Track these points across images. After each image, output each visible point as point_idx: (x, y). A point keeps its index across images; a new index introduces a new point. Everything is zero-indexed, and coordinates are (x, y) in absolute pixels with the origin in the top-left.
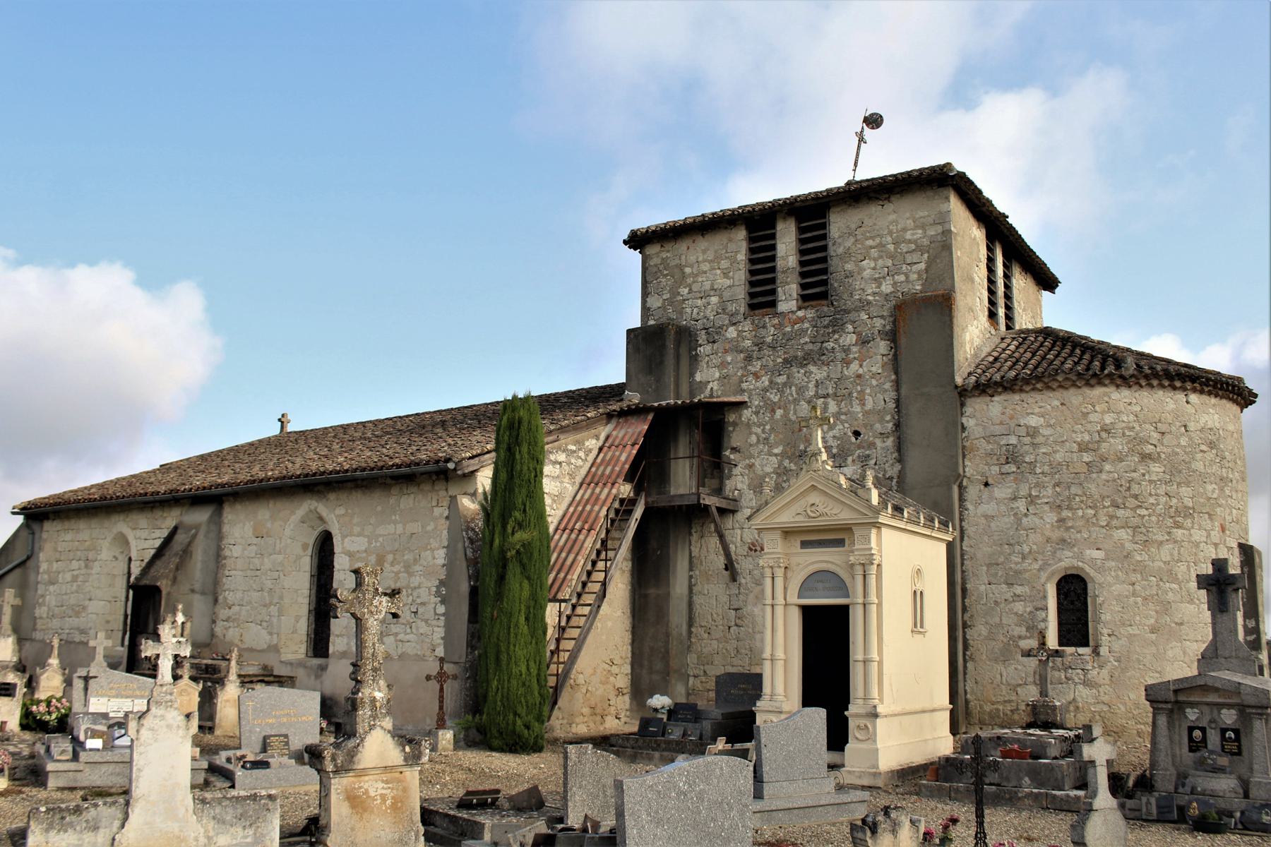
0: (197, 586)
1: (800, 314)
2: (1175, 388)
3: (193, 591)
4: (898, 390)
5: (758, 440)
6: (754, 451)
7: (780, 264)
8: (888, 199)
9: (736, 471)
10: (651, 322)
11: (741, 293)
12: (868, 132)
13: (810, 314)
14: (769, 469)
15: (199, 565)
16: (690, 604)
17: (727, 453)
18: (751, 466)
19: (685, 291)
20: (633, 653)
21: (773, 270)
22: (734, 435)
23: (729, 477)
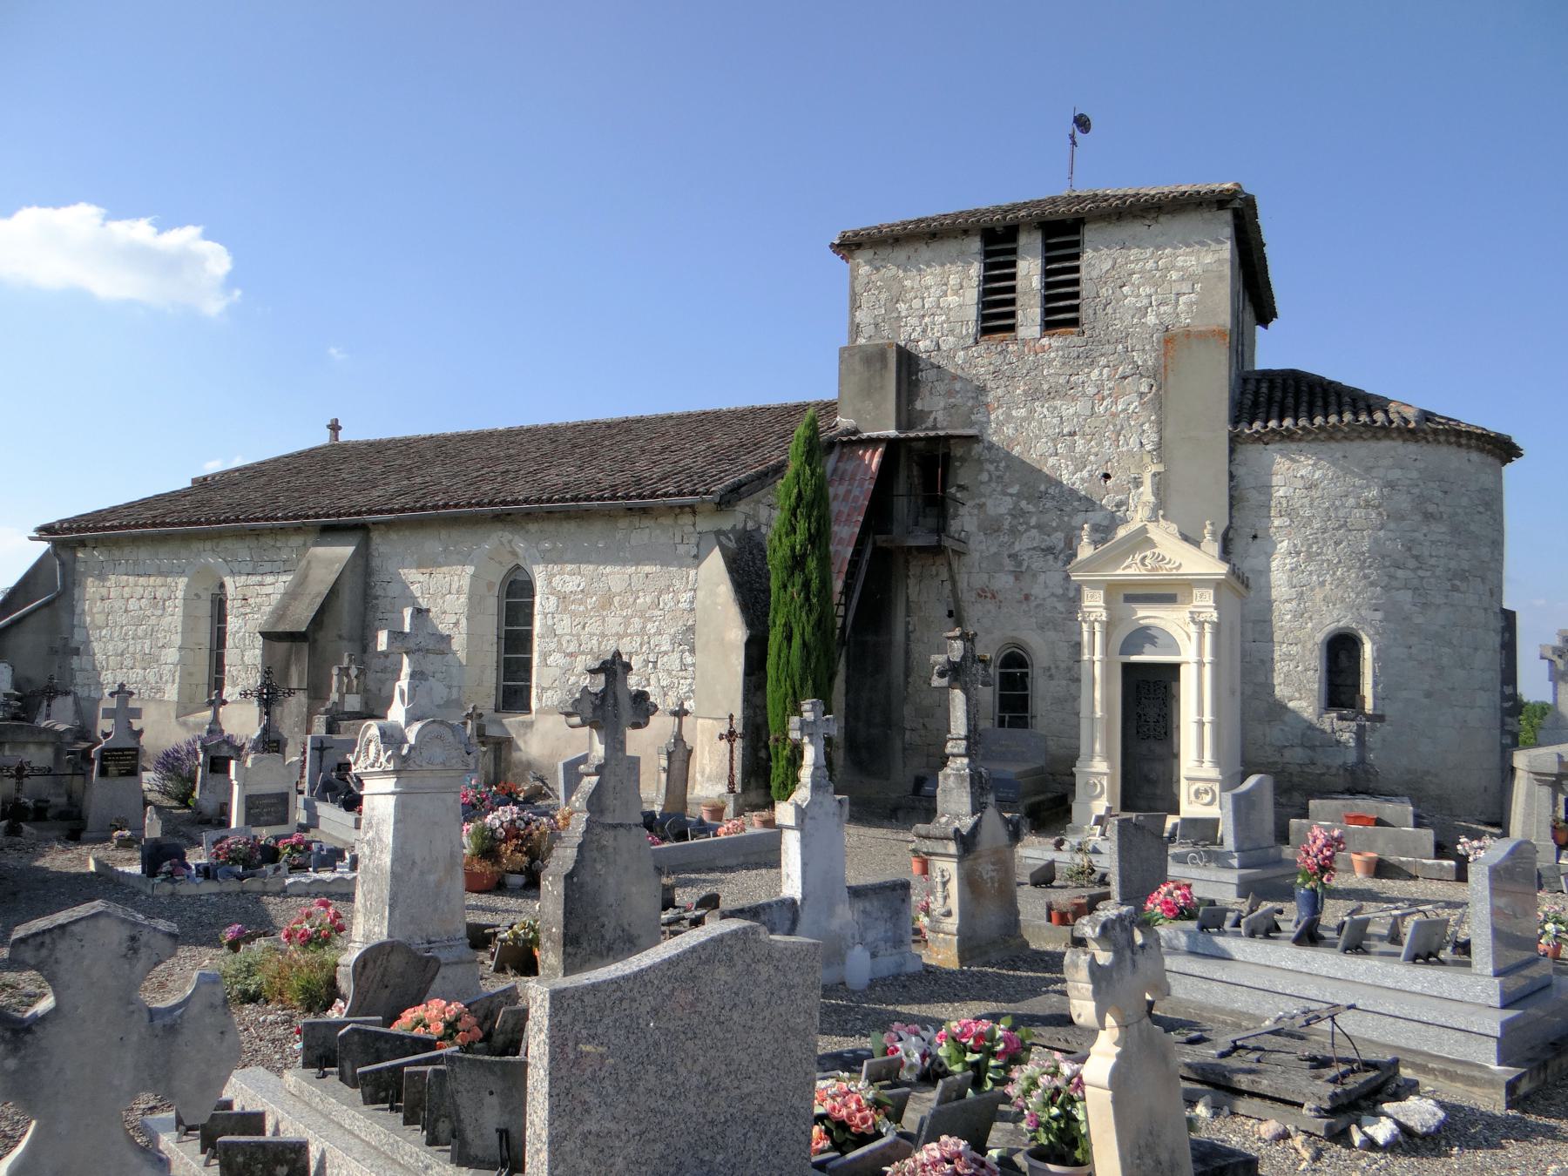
0: (345, 632)
1: (1045, 341)
2: (1460, 445)
3: (340, 637)
4: (1160, 432)
5: (990, 480)
6: (985, 490)
7: (1020, 283)
8: (1156, 219)
9: (963, 511)
10: (861, 341)
11: (972, 313)
12: (1079, 136)
13: (1056, 342)
14: (1003, 510)
15: (346, 606)
16: (907, 653)
17: (953, 490)
18: (981, 506)
19: (902, 306)
20: (847, 705)
21: (1012, 289)
22: (961, 472)
23: (956, 516)
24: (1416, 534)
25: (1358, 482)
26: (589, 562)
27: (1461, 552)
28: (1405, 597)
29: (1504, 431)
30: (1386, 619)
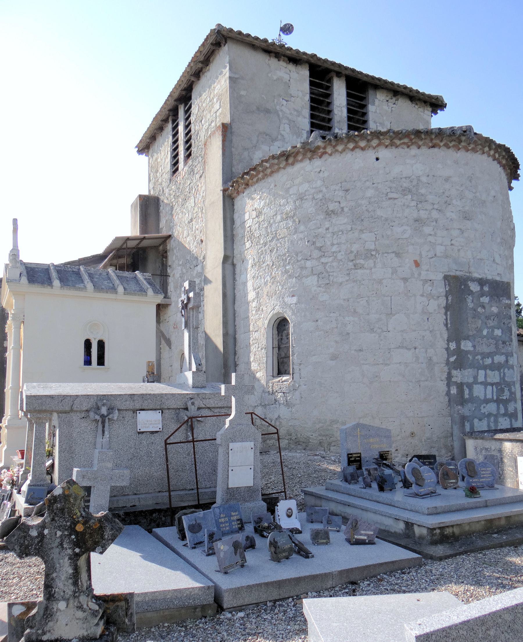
24: (320, 230)
25: (283, 201)
26: (44, 595)
27: (363, 236)
28: (312, 281)
29: (113, 238)
30: (299, 302)
